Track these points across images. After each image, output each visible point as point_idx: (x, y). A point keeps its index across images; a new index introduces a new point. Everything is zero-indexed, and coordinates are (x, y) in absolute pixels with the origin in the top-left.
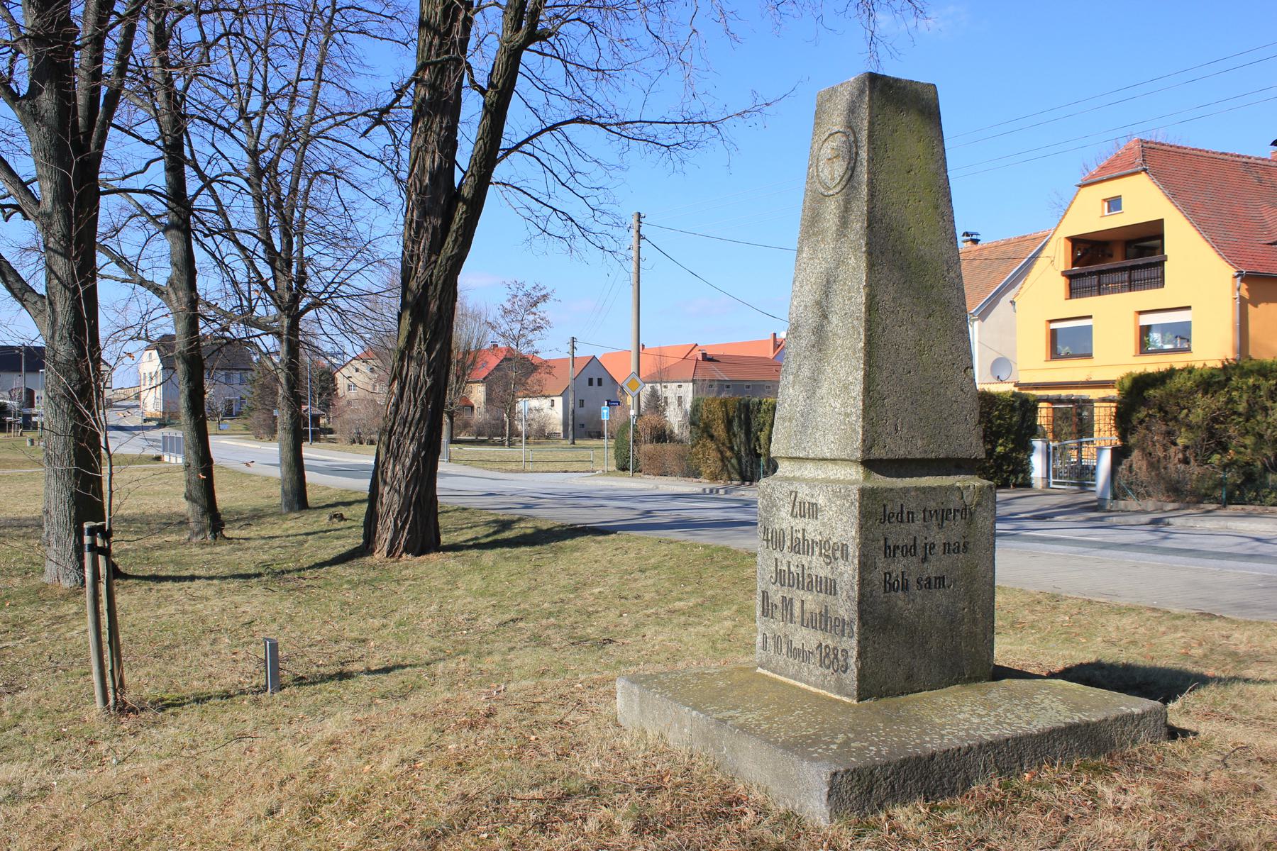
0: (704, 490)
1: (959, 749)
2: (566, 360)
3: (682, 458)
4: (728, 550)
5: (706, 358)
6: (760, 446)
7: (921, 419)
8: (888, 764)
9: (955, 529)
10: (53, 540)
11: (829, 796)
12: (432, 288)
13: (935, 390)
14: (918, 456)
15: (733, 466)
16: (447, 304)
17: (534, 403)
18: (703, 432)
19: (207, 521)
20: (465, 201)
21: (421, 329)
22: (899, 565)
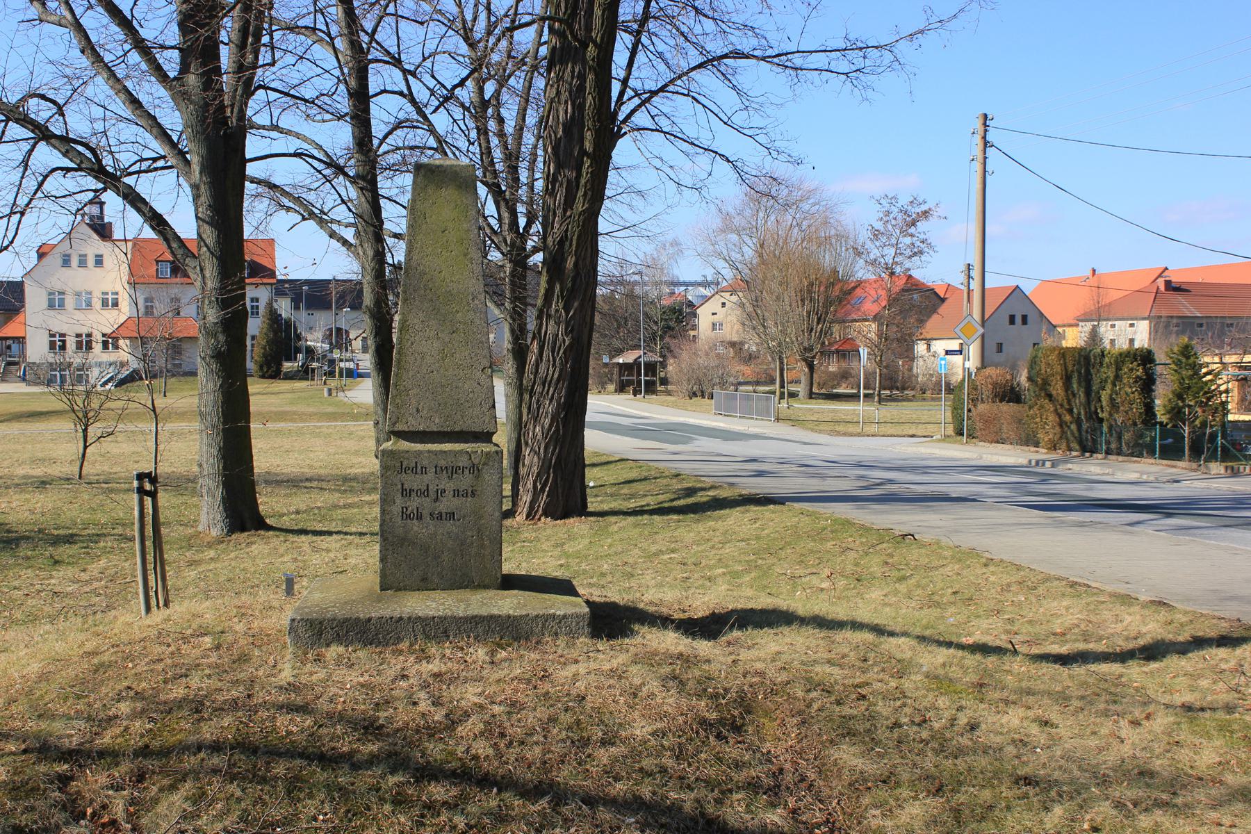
0: (1030, 461)
6: (1102, 407)
8: (334, 619)
9: (465, 481)
10: (204, 491)
12: (568, 243)
15: (1072, 433)
16: (585, 259)
18: (1041, 389)
20: (588, 156)
21: (558, 286)
22: (414, 503)
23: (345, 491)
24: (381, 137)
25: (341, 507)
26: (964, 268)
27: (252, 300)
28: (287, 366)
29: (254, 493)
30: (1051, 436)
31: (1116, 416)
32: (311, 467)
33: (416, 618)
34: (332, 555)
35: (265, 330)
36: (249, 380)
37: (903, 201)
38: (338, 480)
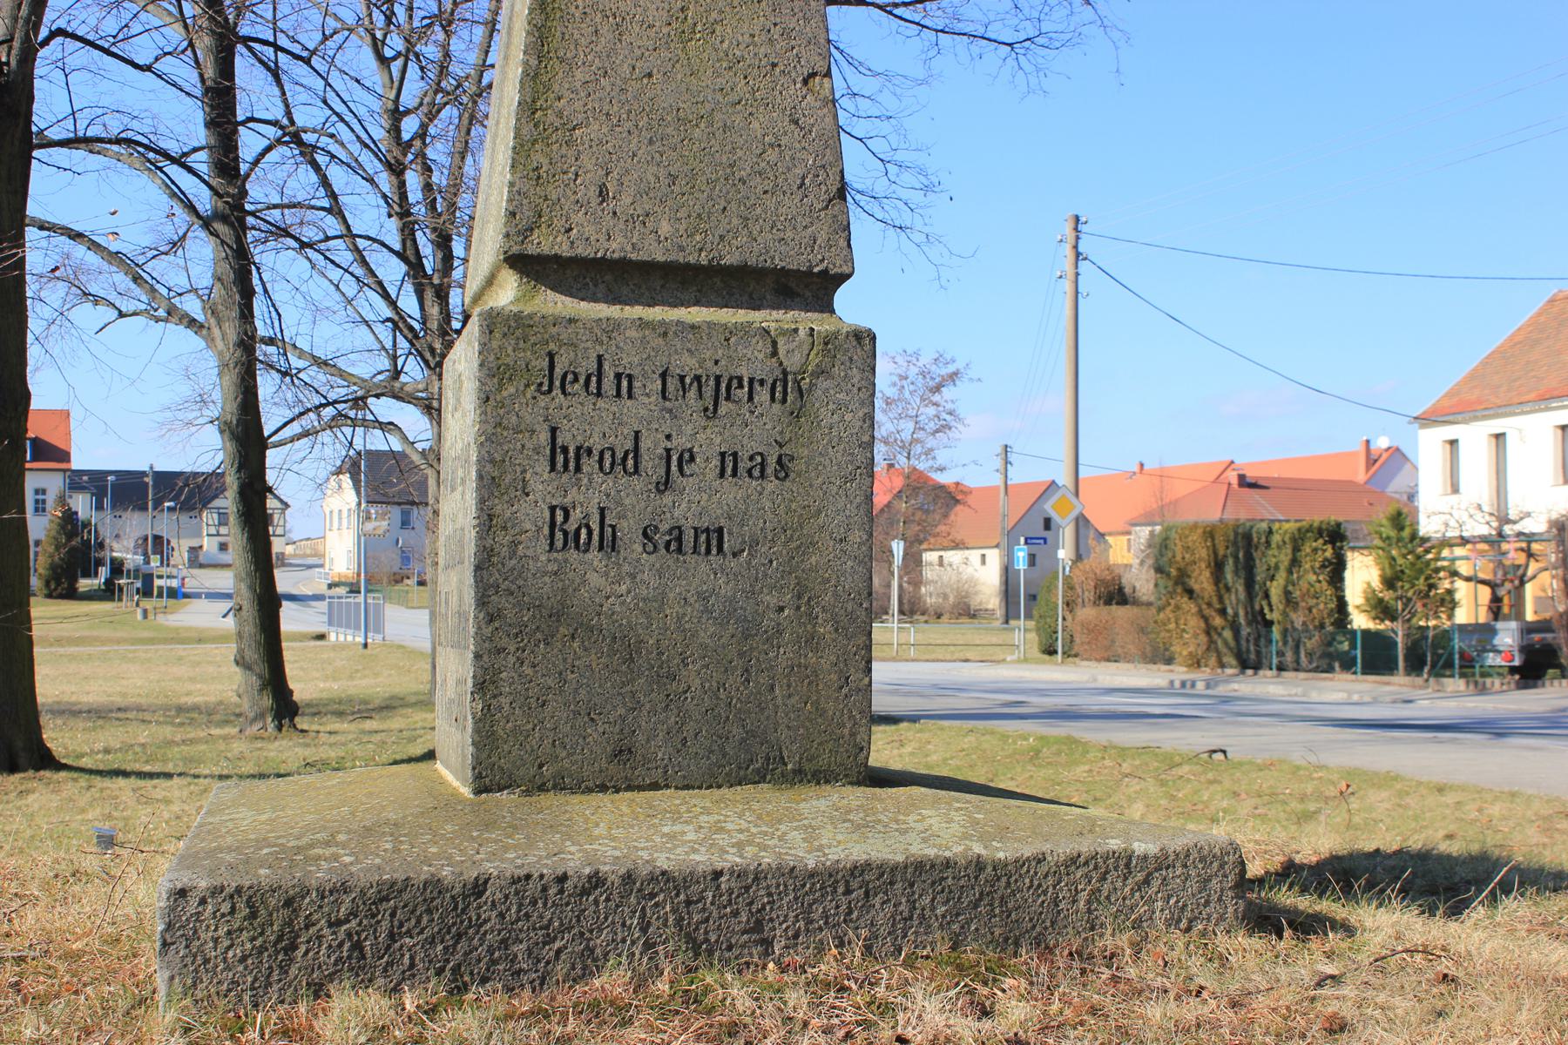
0: (1172, 682)
1: (562, 879)
2: (997, 488)
3: (1143, 630)
4: (1076, 742)
5: (1243, 482)
6: (1270, 605)
7: (673, 179)
8: (345, 888)
11: (165, 944)
13: (718, 116)
14: (660, 258)
15: (1226, 643)
17: (953, 557)
18: (1176, 584)
19: (267, 701)
23: (182, 724)
24: (250, 159)
25: (178, 745)
26: (1000, 450)
27: (37, 492)
28: (84, 584)
29: (39, 728)
30: (1192, 649)
31: (1293, 616)
32: (124, 695)
33: (652, 878)
34: (176, 808)
35: (53, 533)
36: (33, 600)
37: (926, 359)
38: (170, 710)
